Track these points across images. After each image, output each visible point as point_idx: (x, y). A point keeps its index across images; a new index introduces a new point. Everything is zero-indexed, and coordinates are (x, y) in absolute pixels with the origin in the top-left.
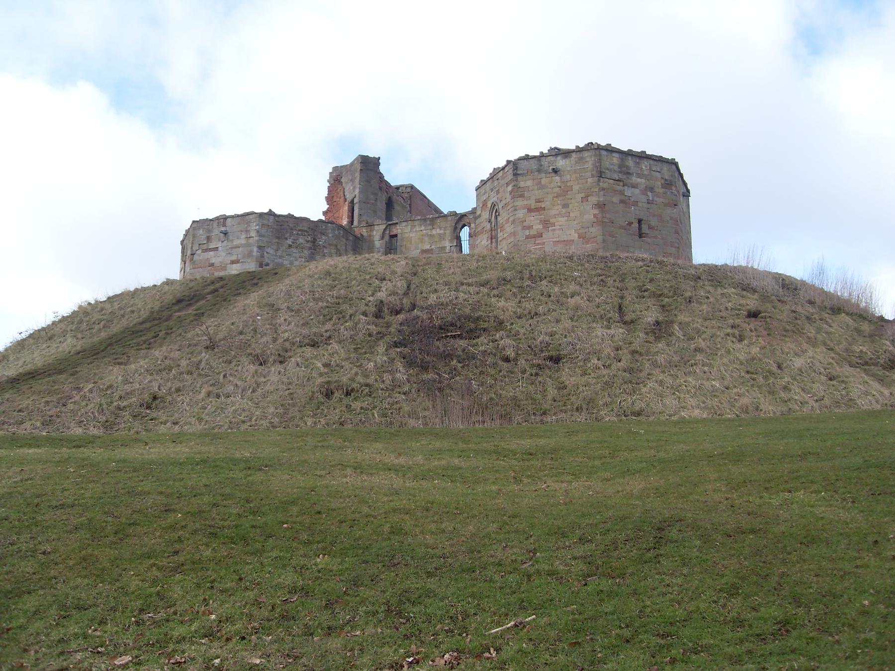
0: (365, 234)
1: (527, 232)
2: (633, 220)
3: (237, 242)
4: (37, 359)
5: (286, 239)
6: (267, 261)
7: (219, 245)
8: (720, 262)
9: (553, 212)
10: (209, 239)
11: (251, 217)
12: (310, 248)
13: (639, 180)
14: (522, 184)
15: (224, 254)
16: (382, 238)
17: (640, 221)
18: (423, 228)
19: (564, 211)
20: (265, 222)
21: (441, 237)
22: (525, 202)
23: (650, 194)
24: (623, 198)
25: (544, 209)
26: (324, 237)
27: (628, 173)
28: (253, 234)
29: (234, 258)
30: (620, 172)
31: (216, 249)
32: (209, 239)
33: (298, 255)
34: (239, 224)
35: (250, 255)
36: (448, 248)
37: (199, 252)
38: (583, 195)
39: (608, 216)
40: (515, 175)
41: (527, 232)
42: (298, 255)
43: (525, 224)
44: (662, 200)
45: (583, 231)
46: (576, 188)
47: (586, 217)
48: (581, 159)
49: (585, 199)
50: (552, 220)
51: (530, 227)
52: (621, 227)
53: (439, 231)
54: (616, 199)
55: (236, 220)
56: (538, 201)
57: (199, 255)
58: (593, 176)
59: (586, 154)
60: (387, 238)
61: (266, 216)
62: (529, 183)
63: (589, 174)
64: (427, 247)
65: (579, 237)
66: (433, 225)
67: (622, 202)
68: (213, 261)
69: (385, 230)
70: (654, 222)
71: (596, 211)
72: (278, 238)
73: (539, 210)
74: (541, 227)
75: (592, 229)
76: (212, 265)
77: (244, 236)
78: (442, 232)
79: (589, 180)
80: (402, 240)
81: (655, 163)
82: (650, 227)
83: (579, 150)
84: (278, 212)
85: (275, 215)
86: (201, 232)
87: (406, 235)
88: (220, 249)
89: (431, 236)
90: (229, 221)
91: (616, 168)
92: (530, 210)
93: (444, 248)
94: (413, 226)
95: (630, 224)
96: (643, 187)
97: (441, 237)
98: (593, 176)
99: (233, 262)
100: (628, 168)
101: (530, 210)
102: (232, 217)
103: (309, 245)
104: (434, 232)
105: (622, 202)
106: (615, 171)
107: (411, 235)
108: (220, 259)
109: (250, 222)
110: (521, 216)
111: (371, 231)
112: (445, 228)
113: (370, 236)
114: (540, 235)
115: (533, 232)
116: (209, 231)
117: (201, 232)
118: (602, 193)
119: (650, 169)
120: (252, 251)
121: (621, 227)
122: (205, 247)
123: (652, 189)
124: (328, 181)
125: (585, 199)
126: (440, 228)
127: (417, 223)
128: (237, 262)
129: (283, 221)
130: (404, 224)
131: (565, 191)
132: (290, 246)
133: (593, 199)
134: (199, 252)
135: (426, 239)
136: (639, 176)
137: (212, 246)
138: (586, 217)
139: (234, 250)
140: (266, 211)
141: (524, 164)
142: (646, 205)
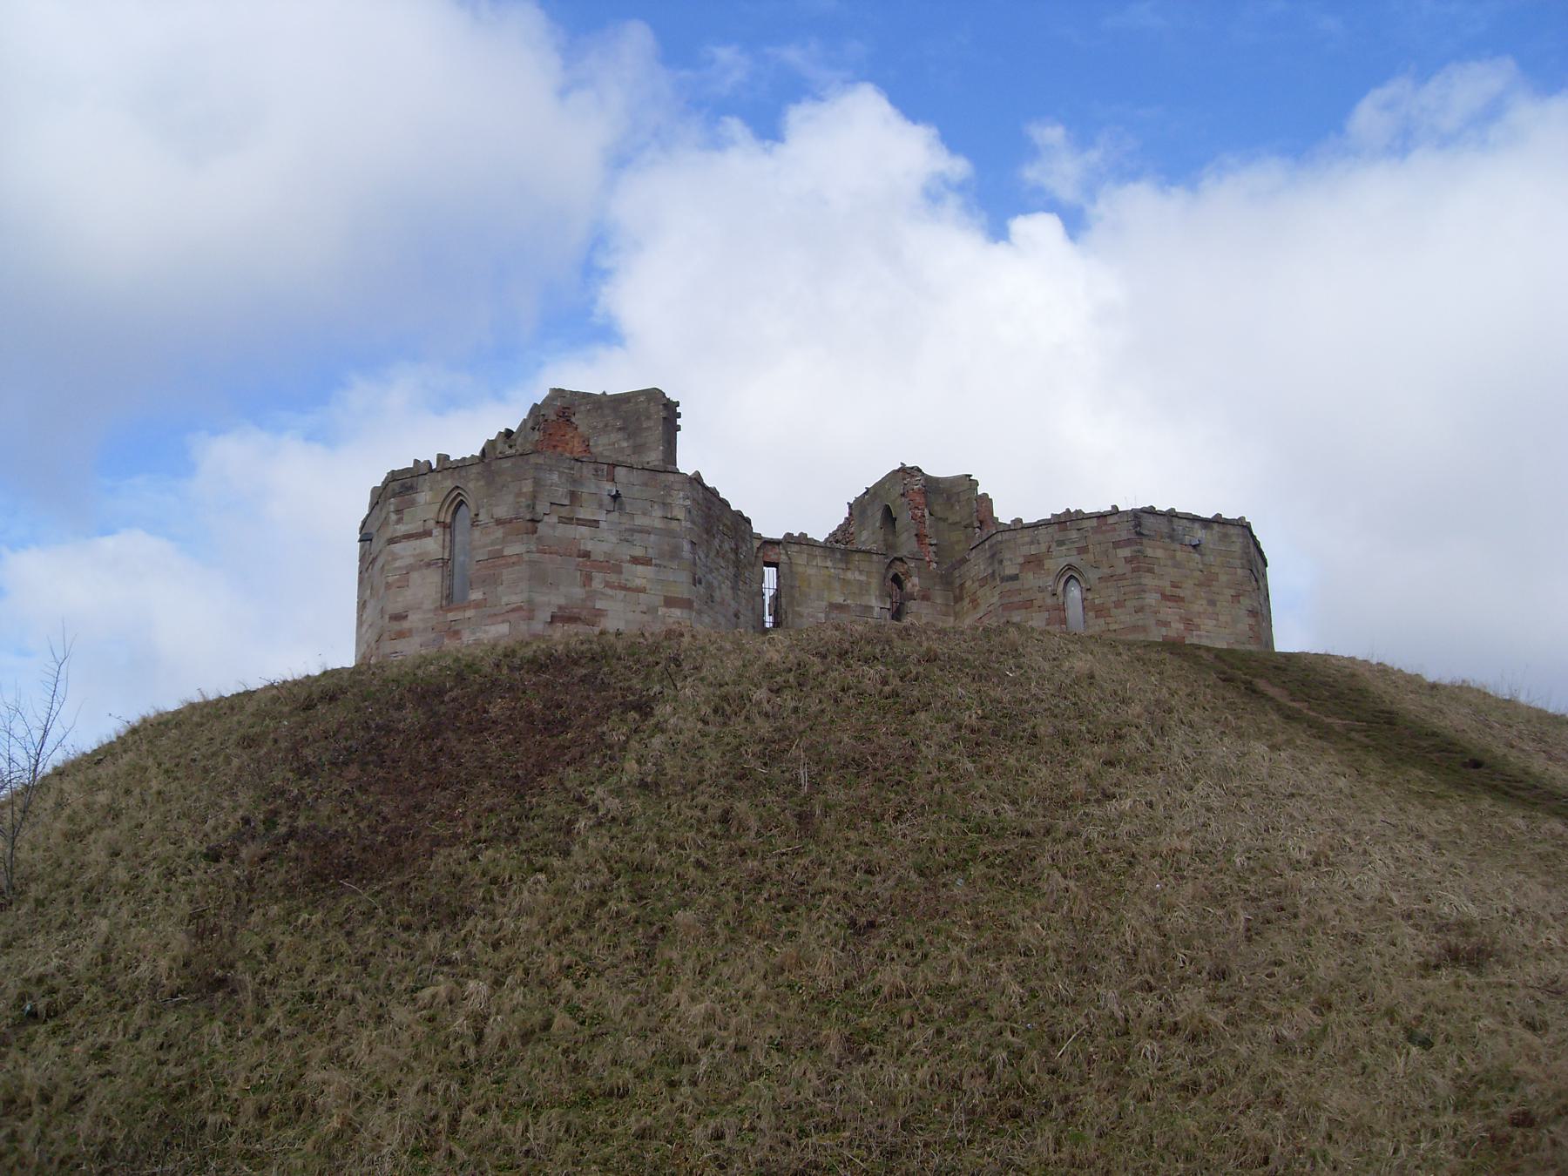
3: (640, 521)
4: (1454, 721)
7: (601, 516)
8: (316, 671)
9: (1196, 608)
14: (1149, 552)
18: (829, 564)
19: (1210, 609)
22: (1156, 582)
25: (1182, 599)
31: (594, 524)
32: (574, 496)
34: (646, 484)
35: (674, 554)
38: (1233, 592)
46: (1223, 578)
49: (1236, 598)
50: (1196, 621)
53: (857, 576)
56: (1174, 585)
57: (553, 527)
59: (1232, 530)
62: (1160, 553)
63: (1238, 562)
66: (847, 563)
73: (1178, 599)
74: (1182, 626)
78: (863, 578)
79: (1239, 571)
86: (555, 477)
88: (602, 524)
89: (845, 582)
93: (869, 608)
97: (863, 588)
99: (635, 560)
101: (1165, 597)
104: (849, 575)
108: (605, 547)
112: (869, 574)
117: (555, 477)
122: (564, 512)
125: (1236, 598)
126: (861, 572)
128: (646, 562)
131: (1207, 581)
135: (837, 585)
137: (584, 513)
139: (637, 536)
141: (1148, 521)
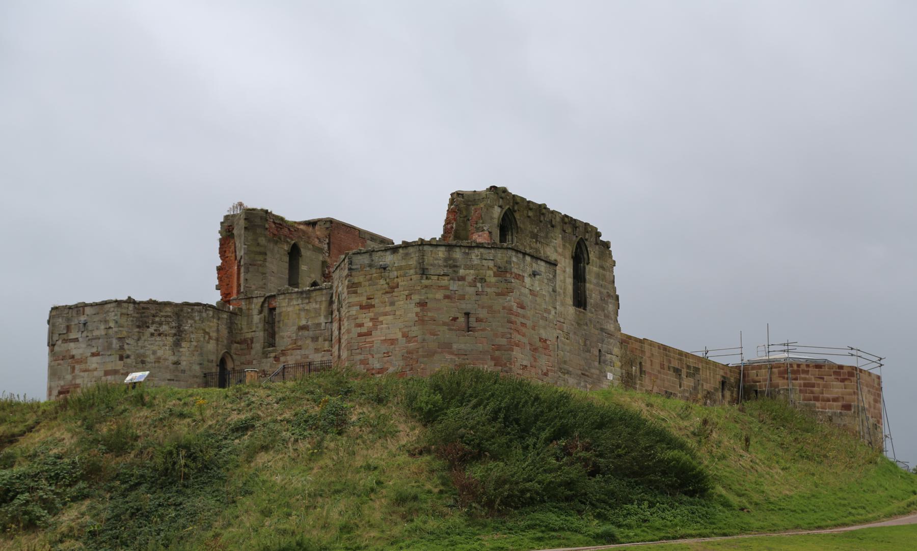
0: (244, 308)
1: (359, 330)
2: (458, 315)
3: (96, 333)
5: (148, 327)
6: (128, 352)
7: (78, 335)
10: (68, 328)
11: (109, 306)
12: (175, 335)
13: (468, 271)
15: (84, 346)
16: (261, 312)
17: (467, 314)
18: (300, 301)
20: (124, 311)
21: (317, 312)
23: (479, 285)
24: (448, 293)
26: (189, 321)
27: (456, 266)
28: (112, 324)
29: (94, 350)
30: (445, 266)
31: (76, 340)
32: (68, 328)
33: (161, 343)
36: (323, 324)
37: (60, 342)
38: (406, 293)
39: (430, 314)
40: (350, 269)
41: (359, 330)
42: (161, 343)
43: (358, 321)
44: (493, 289)
45: (406, 330)
47: (410, 315)
48: (407, 254)
49: (408, 297)
51: (361, 325)
52: (444, 324)
54: (439, 295)
55: (96, 309)
58: (416, 273)
60: (266, 311)
61: (125, 305)
64: (303, 322)
65: (403, 337)
67: (446, 297)
68: (74, 352)
69: (263, 303)
70: (483, 314)
71: (418, 309)
72: (139, 327)
75: (414, 328)
76: (73, 357)
77: (102, 327)
78: (318, 306)
79: (414, 277)
80: (280, 314)
81: (488, 251)
82: (478, 320)
83: (406, 245)
84: (138, 298)
85: (134, 302)
86: (60, 320)
87: (284, 309)
90: (88, 310)
91: (441, 262)
92: (362, 307)
94: (291, 299)
95: (455, 319)
96: (470, 279)
97: (317, 312)
98: (416, 273)
99: (93, 355)
100: (455, 260)
101: (362, 307)
102: (91, 305)
103: (173, 331)
105: (446, 297)
106: (440, 266)
107: (289, 309)
108: (81, 351)
109: (108, 311)
110: (354, 313)
111: (250, 303)
113: (249, 309)
114: (369, 334)
115: (364, 330)
116: (68, 320)
117: (60, 320)
118: (423, 291)
119: (482, 259)
120: (111, 344)
121: (444, 324)
123: (483, 280)
124: (220, 232)
127: (294, 296)
129: (143, 308)
130: (282, 297)
132: (152, 335)
133: (416, 298)
134: (60, 342)
135: (303, 314)
136: (467, 267)
137: (72, 336)
138: (410, 315)
140: (125, 298)
142: (474, 298)
